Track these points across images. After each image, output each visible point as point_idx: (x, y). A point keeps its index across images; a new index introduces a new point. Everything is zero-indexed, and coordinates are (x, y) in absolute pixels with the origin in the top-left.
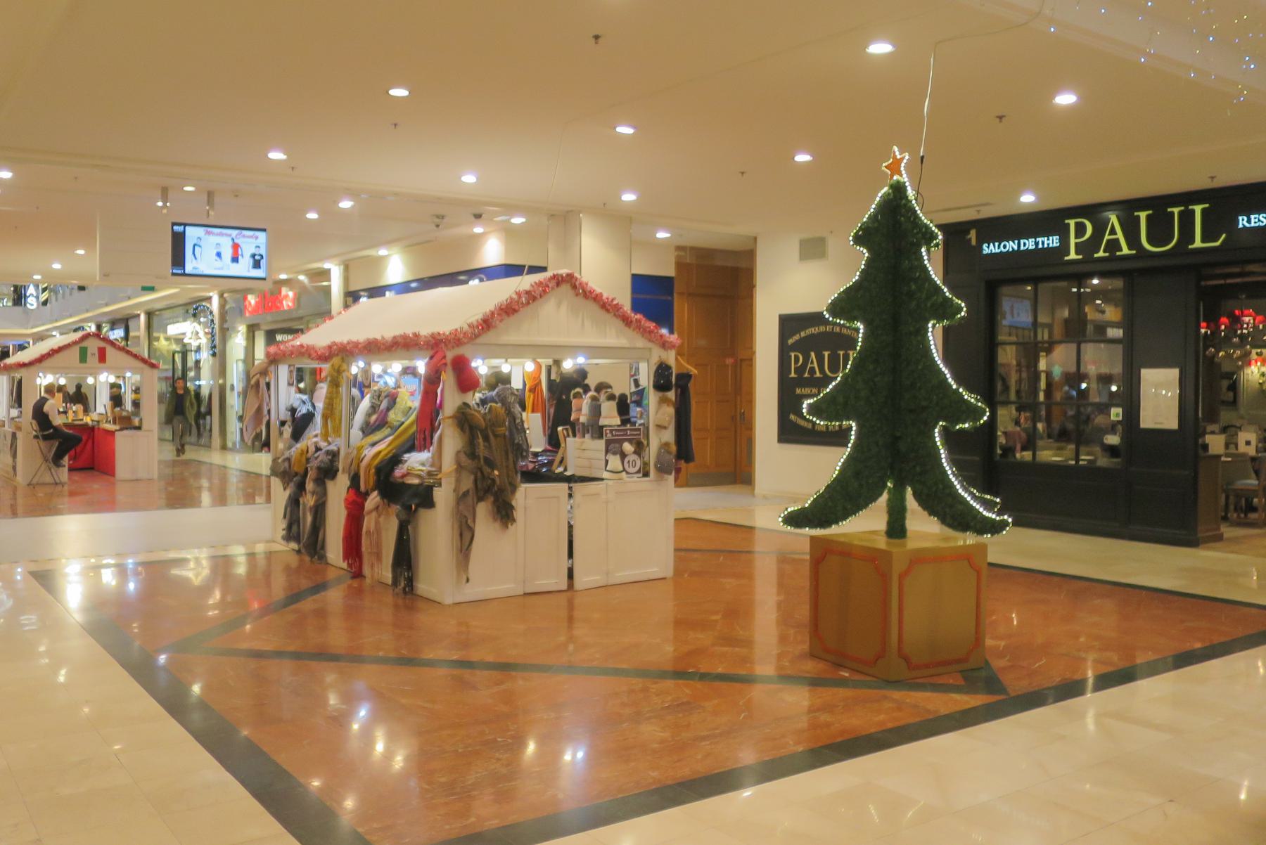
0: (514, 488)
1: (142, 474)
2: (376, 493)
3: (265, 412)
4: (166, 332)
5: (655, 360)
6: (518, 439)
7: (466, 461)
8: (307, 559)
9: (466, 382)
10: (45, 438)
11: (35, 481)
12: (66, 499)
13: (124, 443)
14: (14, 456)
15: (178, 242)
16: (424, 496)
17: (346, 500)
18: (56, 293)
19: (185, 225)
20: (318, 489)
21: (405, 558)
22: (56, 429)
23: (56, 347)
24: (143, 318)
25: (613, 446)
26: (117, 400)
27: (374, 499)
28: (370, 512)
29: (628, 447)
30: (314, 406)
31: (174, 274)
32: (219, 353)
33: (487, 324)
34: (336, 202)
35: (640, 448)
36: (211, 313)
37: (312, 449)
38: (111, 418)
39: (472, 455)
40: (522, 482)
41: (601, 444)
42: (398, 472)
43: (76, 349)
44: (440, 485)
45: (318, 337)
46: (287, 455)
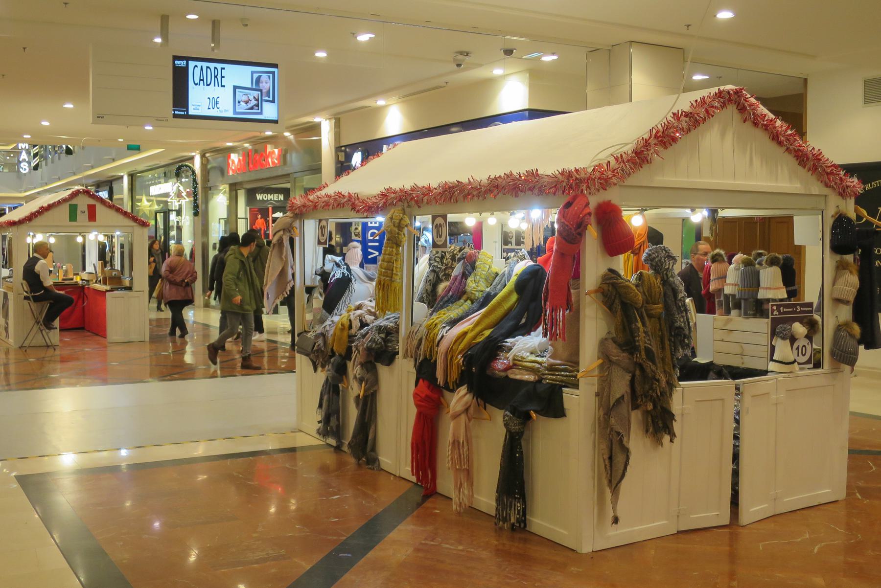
0: (671, 386)
1: (134, 337)
2: (463, 390)
3: (290, 277)
4: (148, 194)
5: (831, 212)
6: (680, 322)
7: (615, 352)
8: (352, 460)
9: (616, 239)
10: (36, 299)
11: (26, 344)
12: (59, 366)
13: (114, 303)
14: (6, 316)
15: (180, 80)
16: (546, 398)
17: (416, 395)
18: (46, 159)
19: (188, 59)
20: (367, 376)
21: (514, 480)
22: (46, 289)
23: (45, 205)
24: (126, 180)
25: (779, 329)
26: (102, 255)
27: (459, 399)
28: (456, 416)
29: (799, 329)
30: (349, 269)
31: (175, 116)
32: (200, 211)
33: (639, 157)
34: (354, 35)
35: (813, 327)
36: (194, 172)
37: (356, 324)
38: (101, 278)
39: (628, 344)
40: (681, 379)
41: (763, 325)
42: (500, 364)
43: (65, 208)
44: (576, 386)
45: (367, 180)
46: (319, 329)
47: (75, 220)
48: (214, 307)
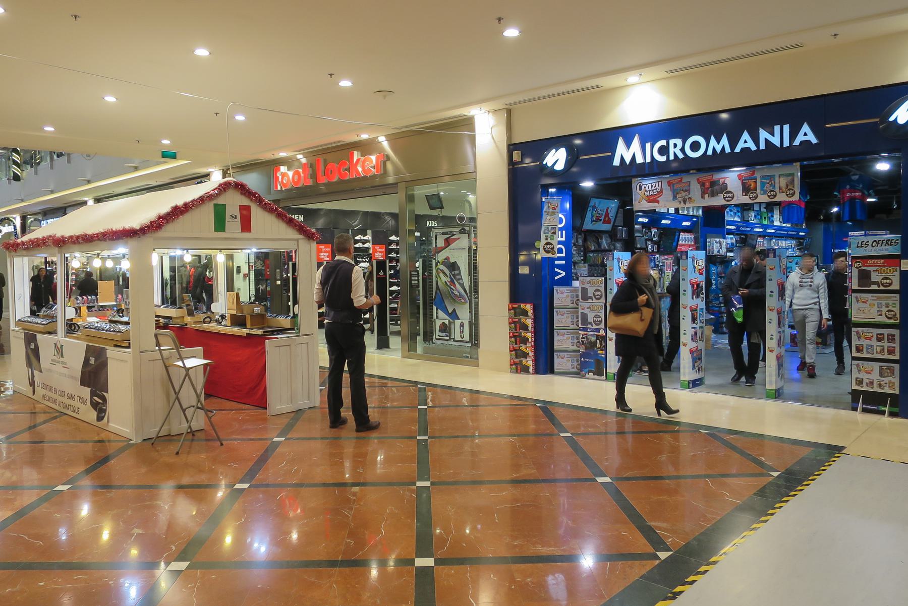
43: (208, 211)
47: (249, 230)
48: (645, 372)
